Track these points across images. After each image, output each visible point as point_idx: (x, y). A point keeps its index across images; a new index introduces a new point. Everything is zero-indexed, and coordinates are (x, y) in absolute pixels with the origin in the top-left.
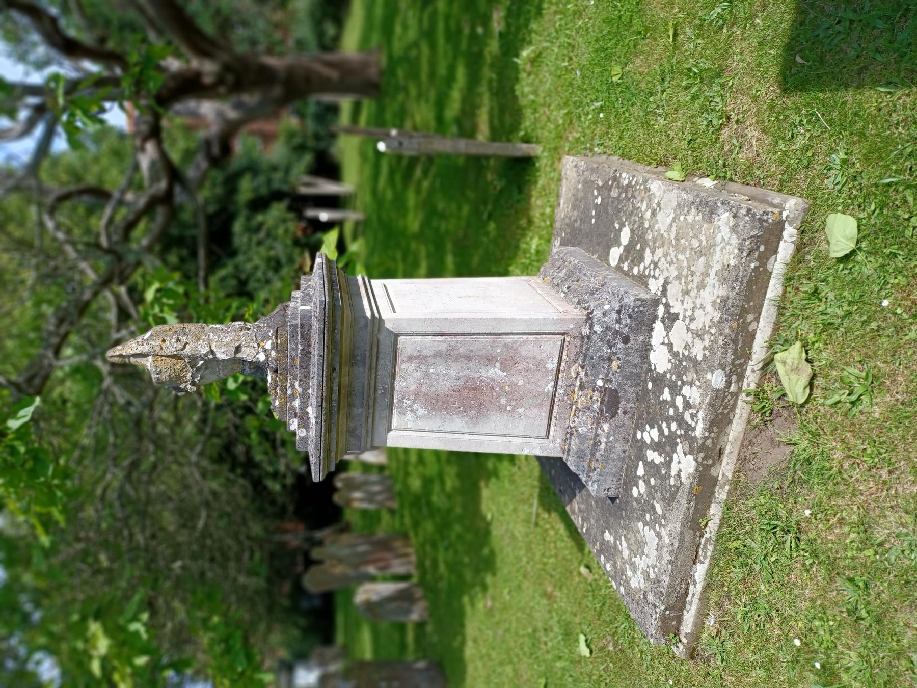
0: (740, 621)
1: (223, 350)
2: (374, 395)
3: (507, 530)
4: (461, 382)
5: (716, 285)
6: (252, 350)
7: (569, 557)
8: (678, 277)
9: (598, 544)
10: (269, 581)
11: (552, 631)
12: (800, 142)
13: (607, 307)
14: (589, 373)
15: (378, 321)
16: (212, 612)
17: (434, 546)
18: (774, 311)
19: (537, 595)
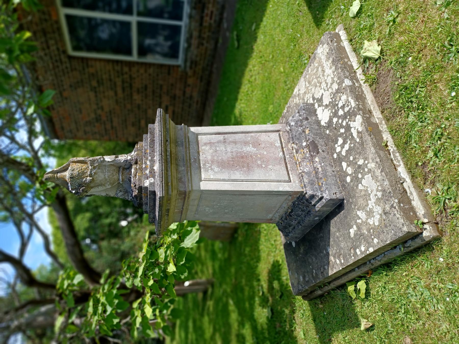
4: (234, 154)
18: (353, 54)
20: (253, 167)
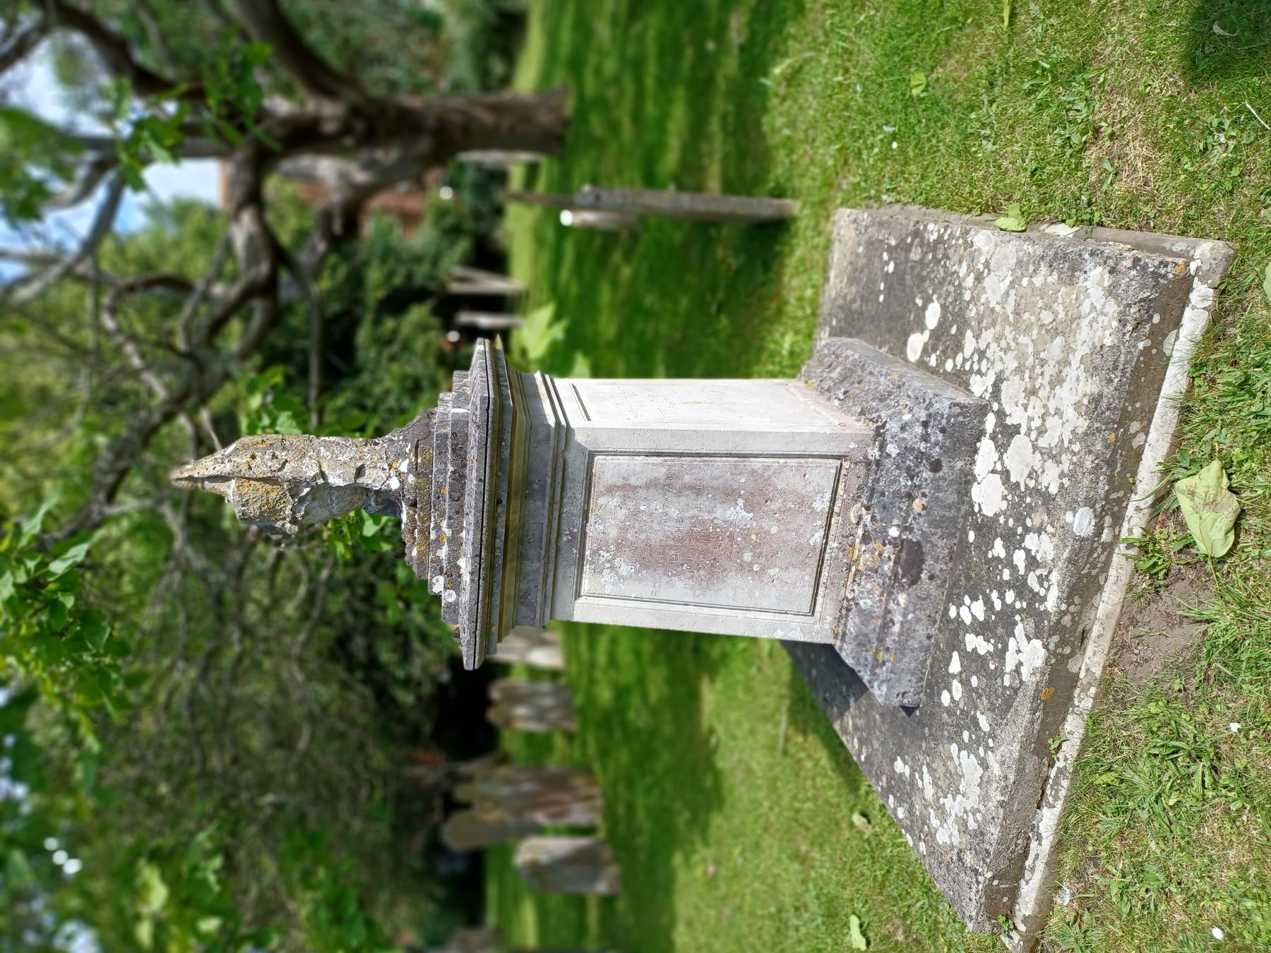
0: (1114, 899)
1: (338, 472)
2: (557, 542)
3: (740, 761)
4: (685, 527)
5: (1082, 378)
6: (381, 473)
7: (835, 800)
8: (1019, 370)
9: (884, 778)
10: (394, 829)
11: (806, 911)
12: (1218, 156)
13: (907, 417)
14: (878, 517)
15: (564, 432)
16: (316, 863)
17: (630, 784)
19: (784, 856)
20: (725, 570)
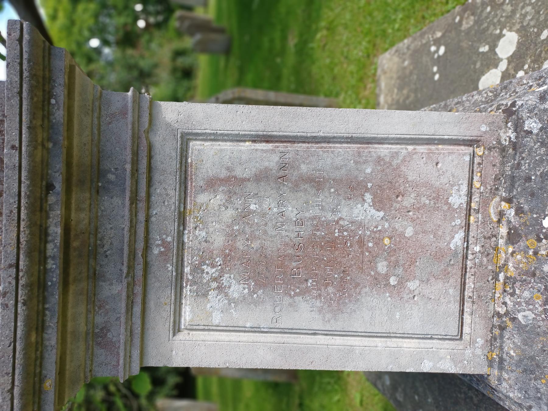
20: (357, 285)
